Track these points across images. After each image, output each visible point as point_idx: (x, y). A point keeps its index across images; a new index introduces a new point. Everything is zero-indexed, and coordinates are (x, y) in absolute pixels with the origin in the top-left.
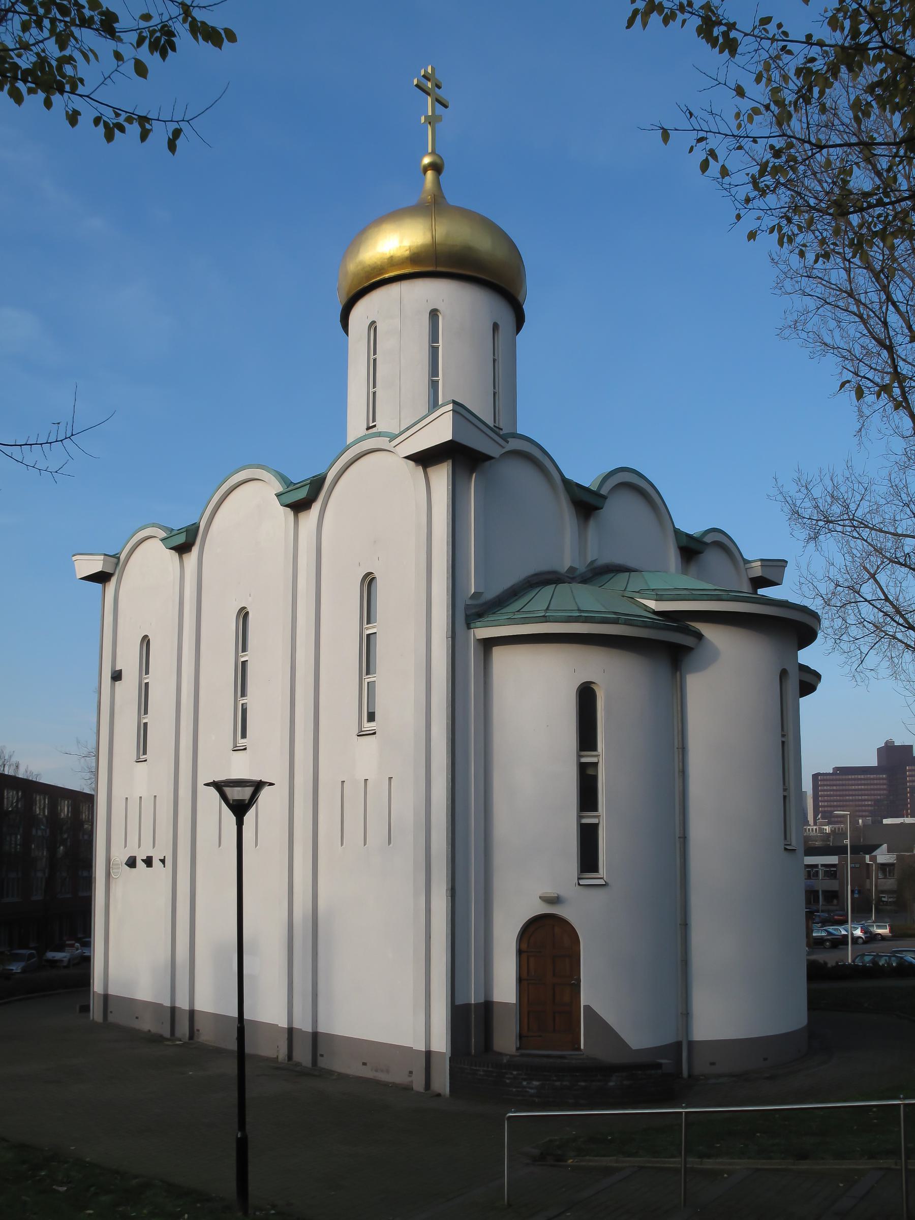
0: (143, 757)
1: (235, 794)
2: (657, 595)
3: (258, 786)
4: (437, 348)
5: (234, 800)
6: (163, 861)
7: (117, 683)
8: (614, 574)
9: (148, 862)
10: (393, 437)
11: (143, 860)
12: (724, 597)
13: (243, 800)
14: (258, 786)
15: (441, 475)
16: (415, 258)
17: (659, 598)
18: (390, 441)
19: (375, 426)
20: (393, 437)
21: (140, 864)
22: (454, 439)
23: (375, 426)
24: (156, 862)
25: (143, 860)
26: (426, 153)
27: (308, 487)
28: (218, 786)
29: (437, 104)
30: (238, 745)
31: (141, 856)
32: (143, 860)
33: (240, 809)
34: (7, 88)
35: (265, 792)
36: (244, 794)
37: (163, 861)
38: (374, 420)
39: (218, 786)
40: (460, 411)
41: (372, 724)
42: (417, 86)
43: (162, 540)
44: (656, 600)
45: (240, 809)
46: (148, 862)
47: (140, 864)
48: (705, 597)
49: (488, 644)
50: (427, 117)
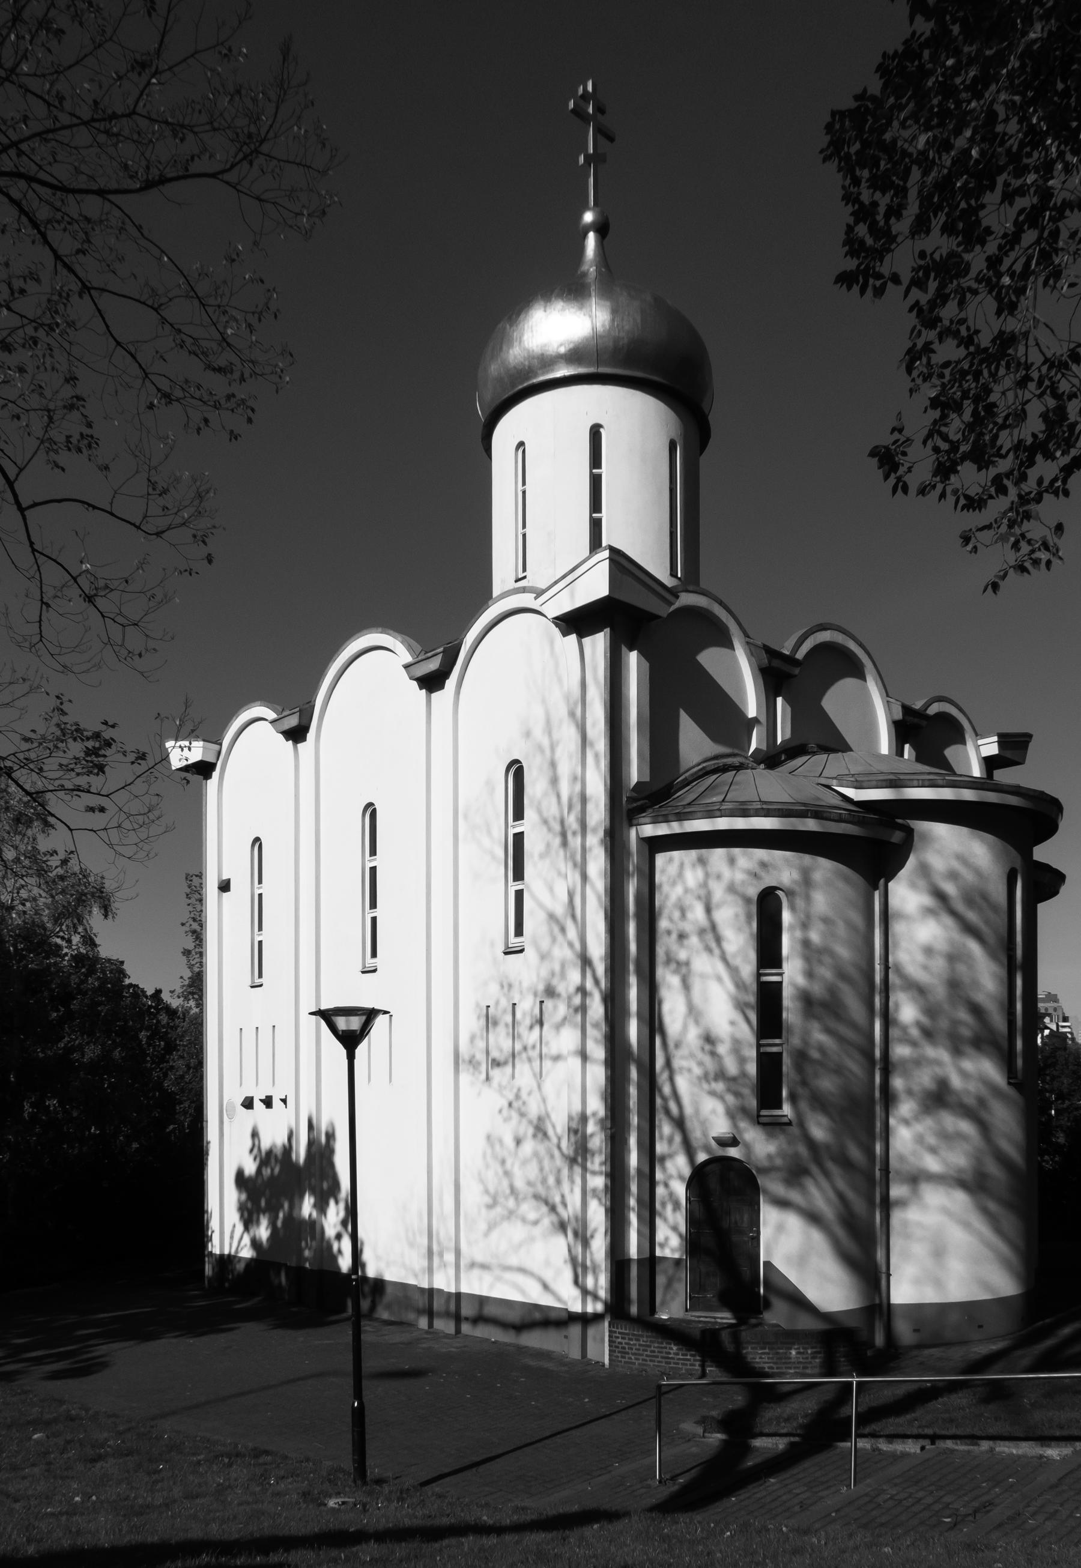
0: (258, 981)
1: (342, 1023)
2: (857, 781)
3: (370, 1015)
4: (599, 476)
5: (343, 1031)
6: (284, 1101)
7: (225, 895)
8: (809, 757)
9: (268, 1102)
10: (539, 593)
11: (261, 1100)
12: (940, 782)
13: (354, 1031)
14: (370, 1015)
15: (598, 643)
16: (575, 355)
17: (859, 786)
18: (536, 598)
19: (525, 577)
20: (539, 593)
21: (258, 1105)
22: (616, 596)
23: (525, 577)
24: (276, 1102)
25: (261, 1100)
26: (586, 208)
27: (440, 656)
28: (327, 1016)
29: (599, 136)
30: (510, 946)
31: (258, 1095)
32: (261, 1100)
33: (350, 1041)
34: (924, 27)
35: (380, 1021)
36: (355, 1023)
37: (284, 1101)
38: (524, 570)
39: (327, 1016)
40: (620, 563)
41: (374, 960)
42: (573, 111)
43: (272, 722)
44: (856, 788)
45: (350, 1041)
46: (268, 1102)
47: (258, 1105)
48: (927, 783)
49: (656, 845)
50: (587, 156)
